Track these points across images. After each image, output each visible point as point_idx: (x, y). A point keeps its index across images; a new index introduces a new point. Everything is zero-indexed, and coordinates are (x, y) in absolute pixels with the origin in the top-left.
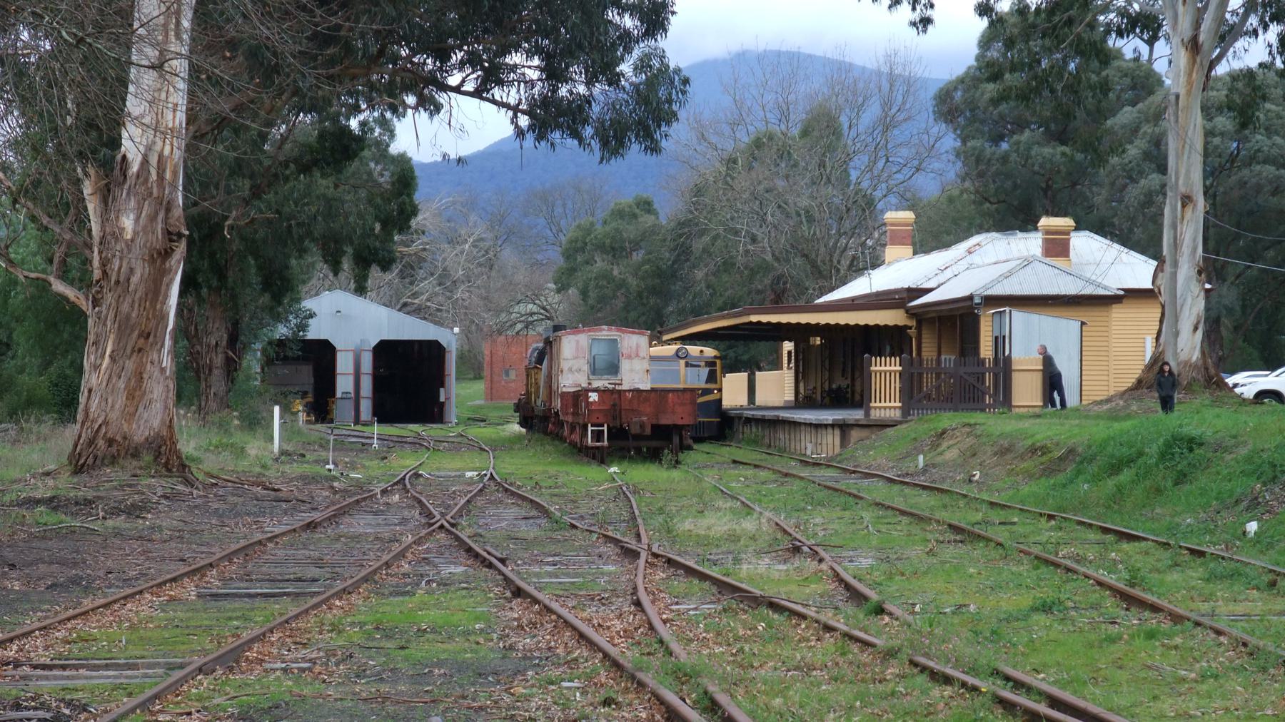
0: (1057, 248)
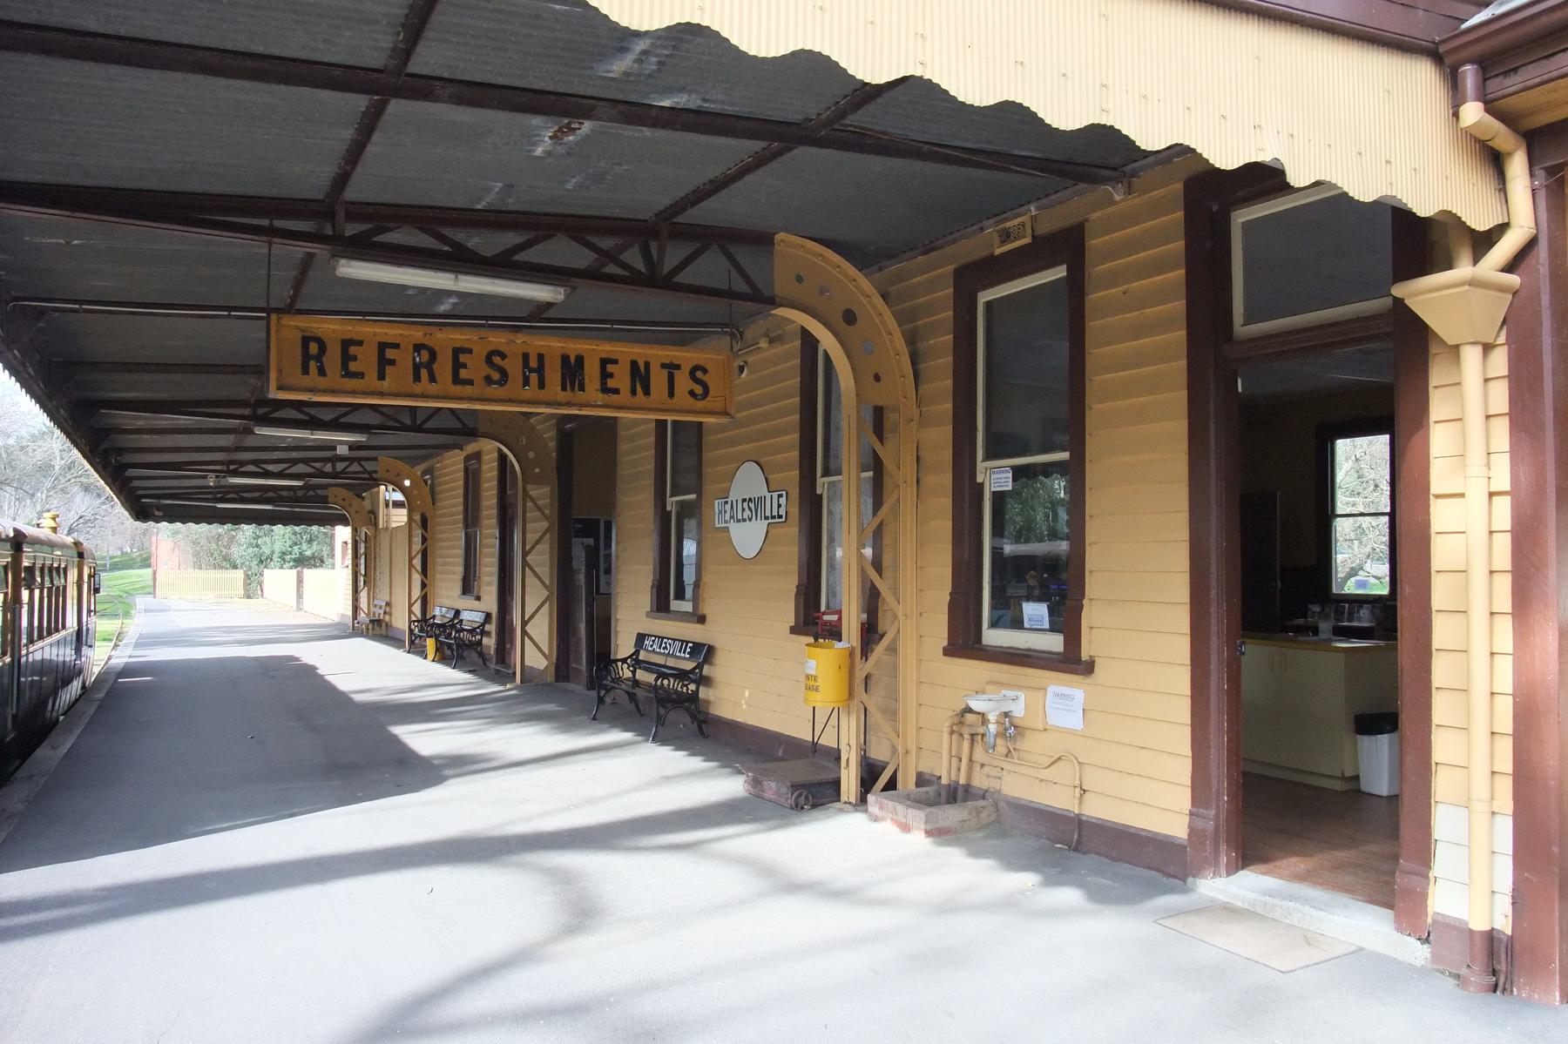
0: (252, 587)
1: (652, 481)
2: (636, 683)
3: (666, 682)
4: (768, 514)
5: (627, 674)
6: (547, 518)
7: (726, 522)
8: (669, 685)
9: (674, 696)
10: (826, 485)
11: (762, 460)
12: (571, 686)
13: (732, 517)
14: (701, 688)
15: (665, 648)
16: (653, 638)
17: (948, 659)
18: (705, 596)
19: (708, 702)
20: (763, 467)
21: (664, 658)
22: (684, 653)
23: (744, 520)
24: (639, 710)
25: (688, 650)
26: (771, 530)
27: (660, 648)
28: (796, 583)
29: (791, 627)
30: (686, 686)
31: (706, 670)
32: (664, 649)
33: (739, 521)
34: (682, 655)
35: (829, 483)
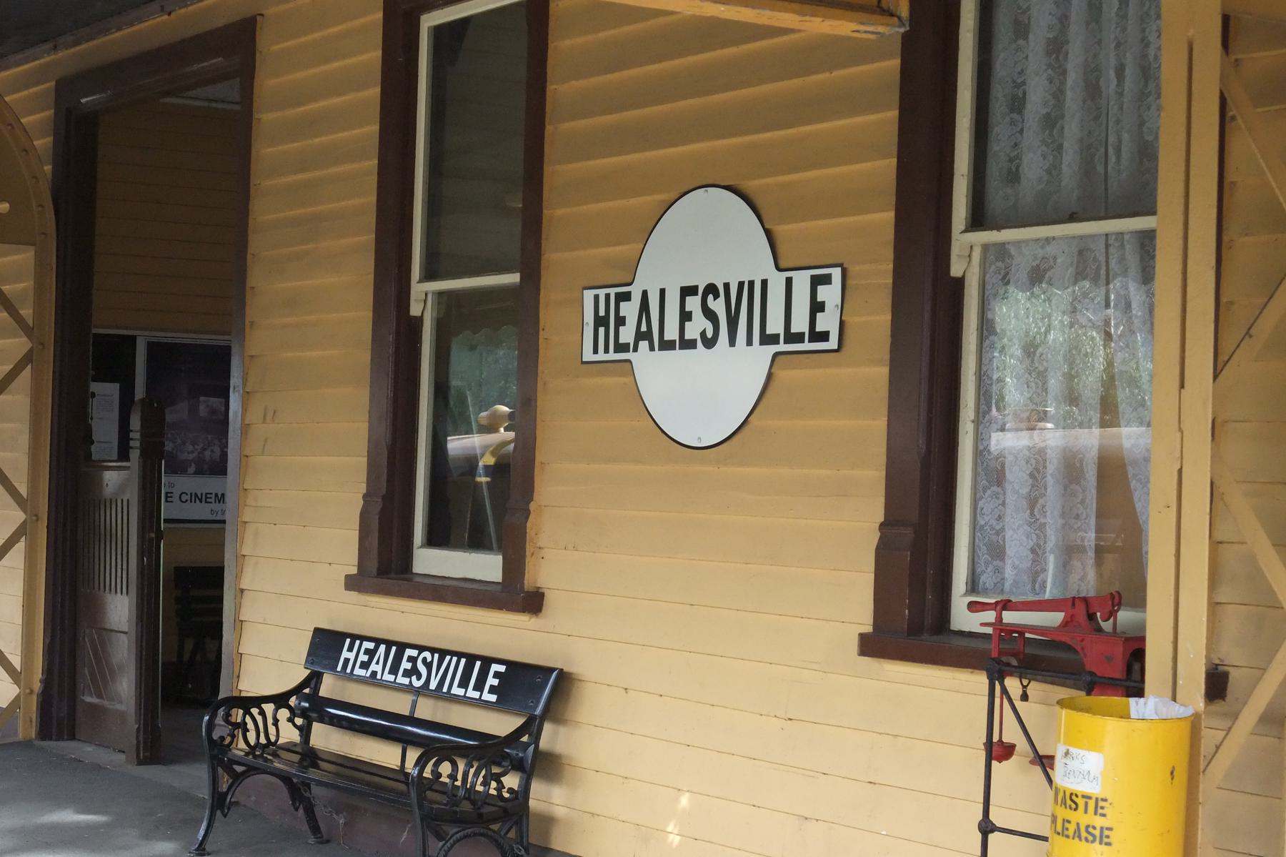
1: (369, 238)
2: (310, 757)
3: (445, 768)
4: (775, 325)
5: (289, 734)
6: (28, 331)
7: (622, 348)
8: (453, 777)
9: (466, 806)
10: (430, 297)
11: (750, 185)
12: (86, 751)
13: (640, 336)
14: (537, 788)
15: (414, 672)
16: (371, 645)
17: (353, 595)
18: (543, 540)
19: (548, 821)
20: (763, 213)
21: (409, 698)
22: (479, 687)
23: (688, 344)
24: (315, 829)
25: (492, 681)
26: (782, 375)
27: (394, 670)
28: (880, 518)
29: (348, 577)
30: (497, 778)
31: (550, 737)
32: (407, 674)
33: (667, 345)
34: (473, 694)
35: (986, 248)
